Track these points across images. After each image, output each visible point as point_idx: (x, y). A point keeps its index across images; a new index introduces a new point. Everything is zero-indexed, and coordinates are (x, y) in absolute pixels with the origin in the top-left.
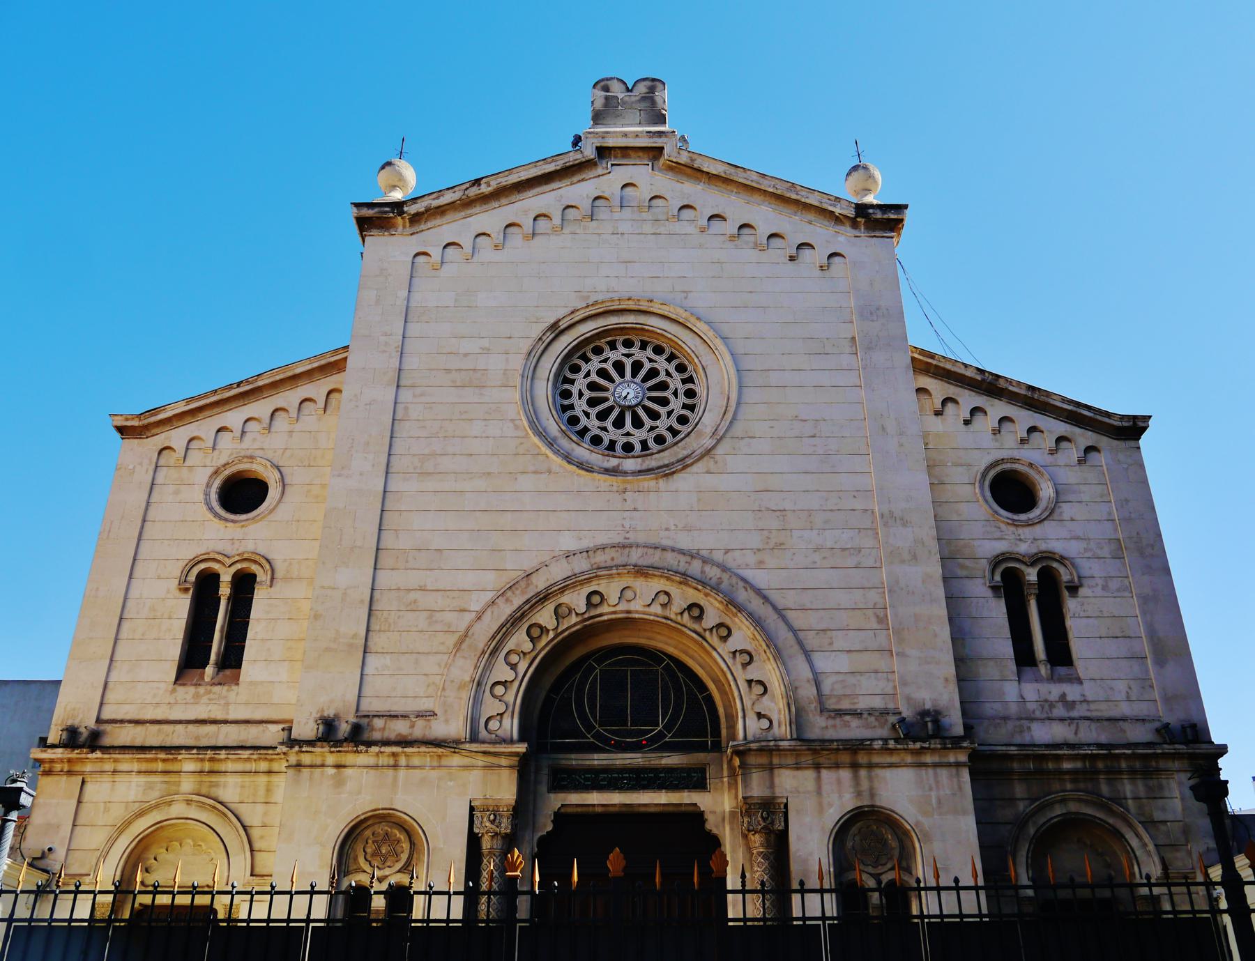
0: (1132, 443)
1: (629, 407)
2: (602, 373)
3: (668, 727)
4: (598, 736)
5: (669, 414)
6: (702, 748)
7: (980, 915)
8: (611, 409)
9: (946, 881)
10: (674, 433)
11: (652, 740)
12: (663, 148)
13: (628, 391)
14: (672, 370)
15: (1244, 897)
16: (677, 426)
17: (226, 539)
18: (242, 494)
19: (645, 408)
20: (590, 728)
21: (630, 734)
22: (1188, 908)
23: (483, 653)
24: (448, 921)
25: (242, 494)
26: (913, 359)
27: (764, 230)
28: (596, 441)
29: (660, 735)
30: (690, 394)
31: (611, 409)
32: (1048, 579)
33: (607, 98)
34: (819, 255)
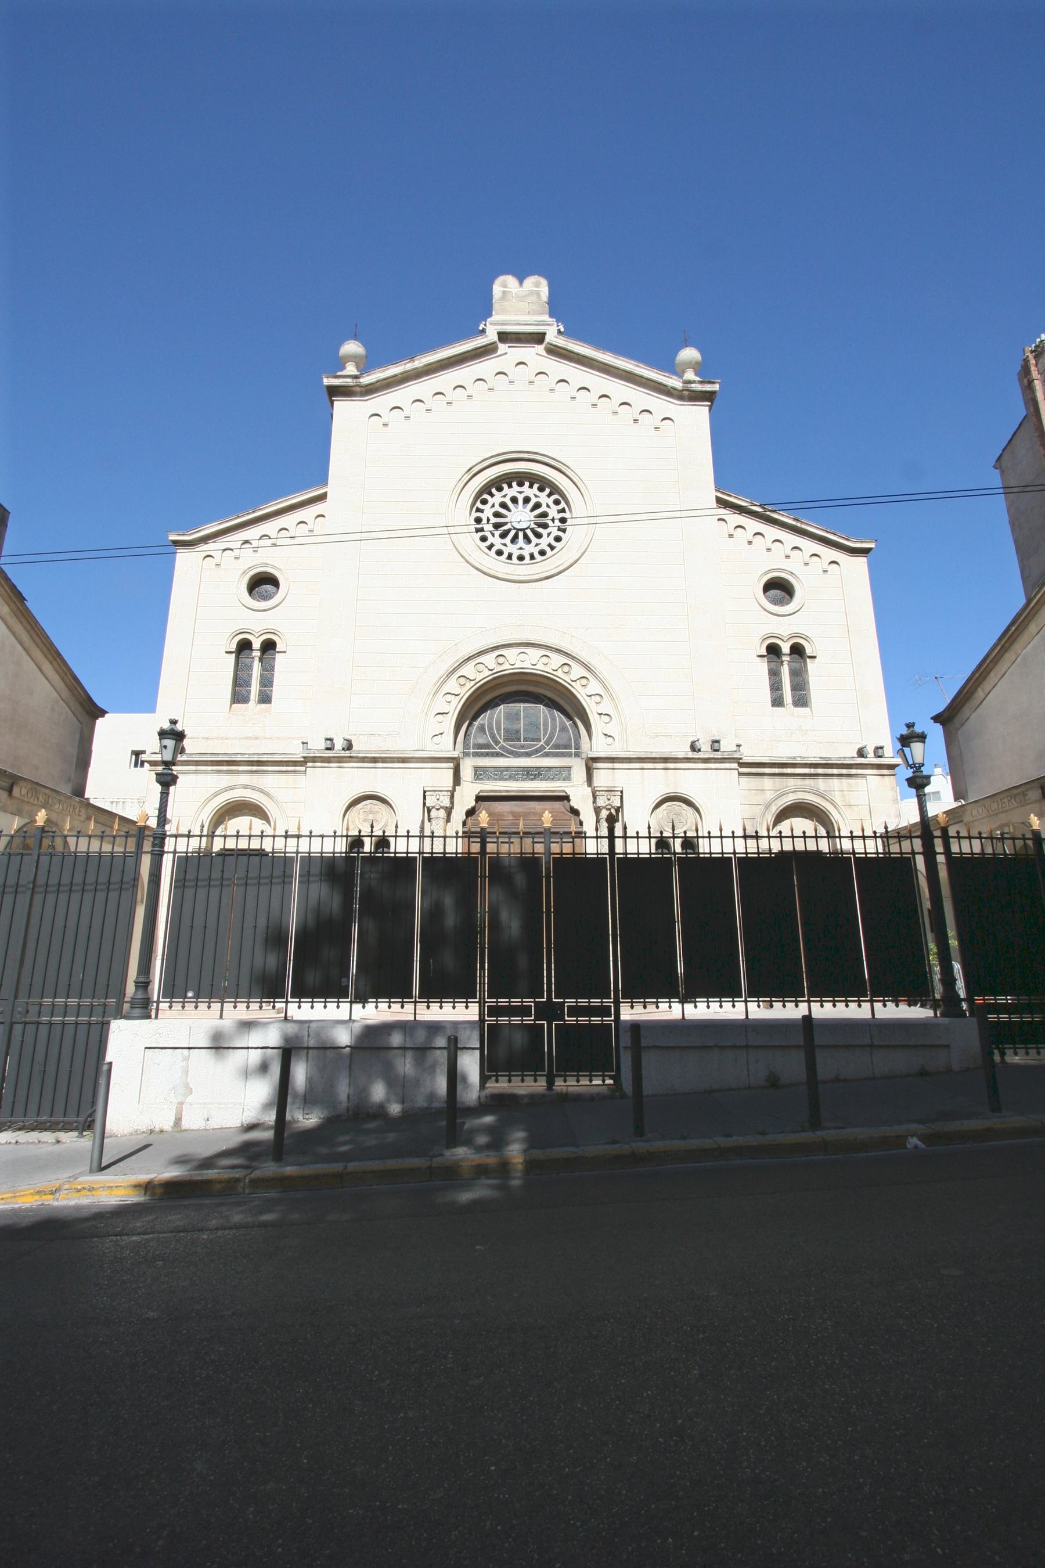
0: (245, 981)
1: (521, 530)
2: (503, 505)
3: (547, 743)
4: (502, 748)
5: (549, 534)
6: (570, 755)
7: (877, 853)
8: (509, 531)
9: (750, 832)
10: (552, 548)
11: (537, 751)
12: (545, 334)
13: (521, 517)
14: (551, 503)
15: (923, 846)
16: (554, 543)
17: (257, 620)
18: (262, 583)
19: (533, 530)
20: (497, 742)
21: (522, 747)
22: (991, 851)
23: (429, 694)
24: (457, 853)
25: (262, 583)
26: (717, 497)
27: (617, 399)
28: (499, 553)
29: (542, 748)
30: (558, 539)
31: (509, 531)
32: (797, 650)
33: (504, 293)
34: (655, 419)
